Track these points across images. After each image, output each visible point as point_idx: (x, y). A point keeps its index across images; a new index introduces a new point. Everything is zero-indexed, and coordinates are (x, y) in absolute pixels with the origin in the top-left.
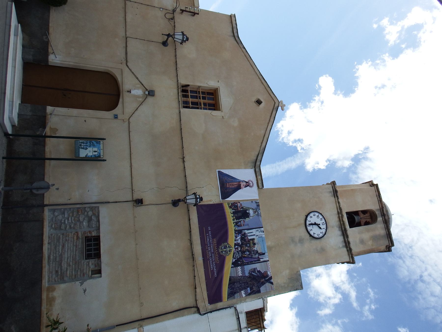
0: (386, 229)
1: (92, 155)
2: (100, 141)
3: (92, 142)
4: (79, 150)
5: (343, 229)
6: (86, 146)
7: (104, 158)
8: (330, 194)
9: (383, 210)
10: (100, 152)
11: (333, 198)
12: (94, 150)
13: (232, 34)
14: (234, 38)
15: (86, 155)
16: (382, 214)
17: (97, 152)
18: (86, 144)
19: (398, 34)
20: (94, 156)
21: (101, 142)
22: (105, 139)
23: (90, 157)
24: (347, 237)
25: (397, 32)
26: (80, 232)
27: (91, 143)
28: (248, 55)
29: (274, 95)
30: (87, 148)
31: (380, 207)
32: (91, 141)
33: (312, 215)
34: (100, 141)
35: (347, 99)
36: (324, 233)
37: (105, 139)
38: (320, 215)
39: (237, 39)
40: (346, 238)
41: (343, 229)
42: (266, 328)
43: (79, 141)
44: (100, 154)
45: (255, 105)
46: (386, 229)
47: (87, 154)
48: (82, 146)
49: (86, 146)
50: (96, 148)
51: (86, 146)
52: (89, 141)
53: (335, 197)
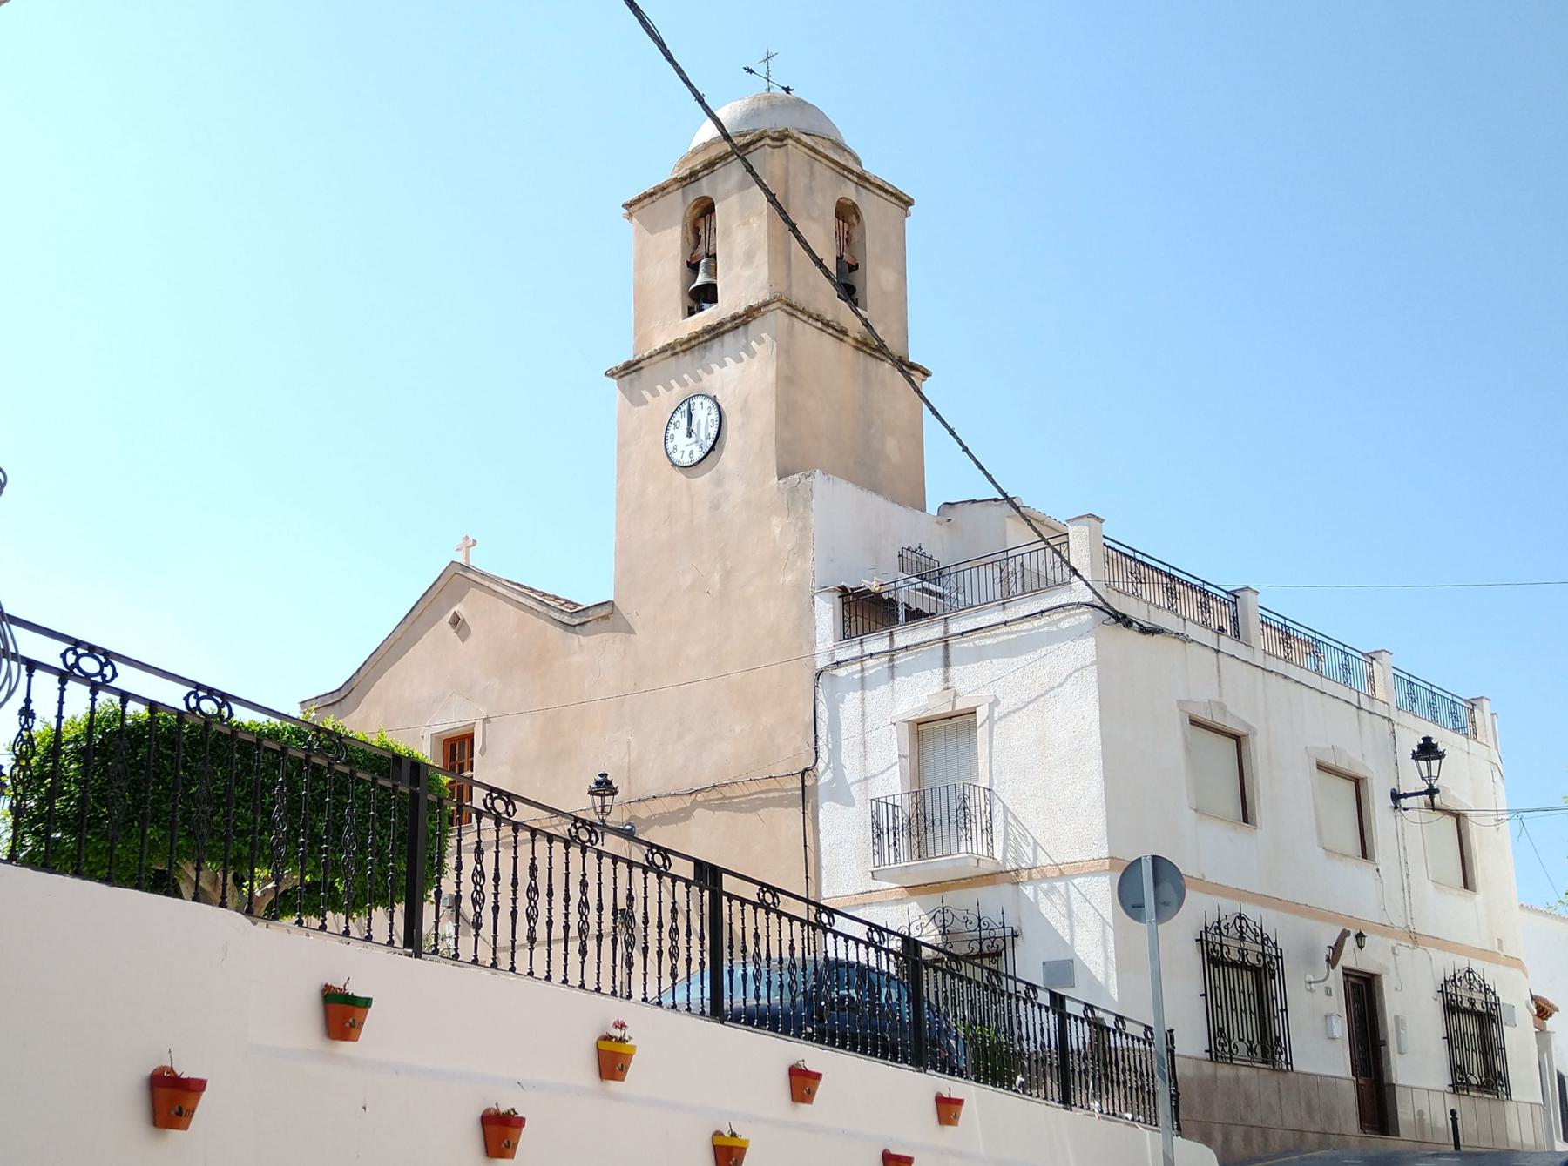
0: (728, 161)
5: (707, 337)
8: (636, 383)
9: (684, 179)
11: (643, 371)
13: (338, 705)
14: (343, 701)
16: (693, 179)
26: (1217, 1126)
28: (438, 584)
29: (439, 578)
31: (678, 189)
33: (686, 461)
35: (59, 655)
36: (694, 458)
38: (670, 449)
39: (343, 694)
40: (726, 327)
41: (707, 337)
45: (132, 1103)
46: (728, 161)
53: (641, 368)
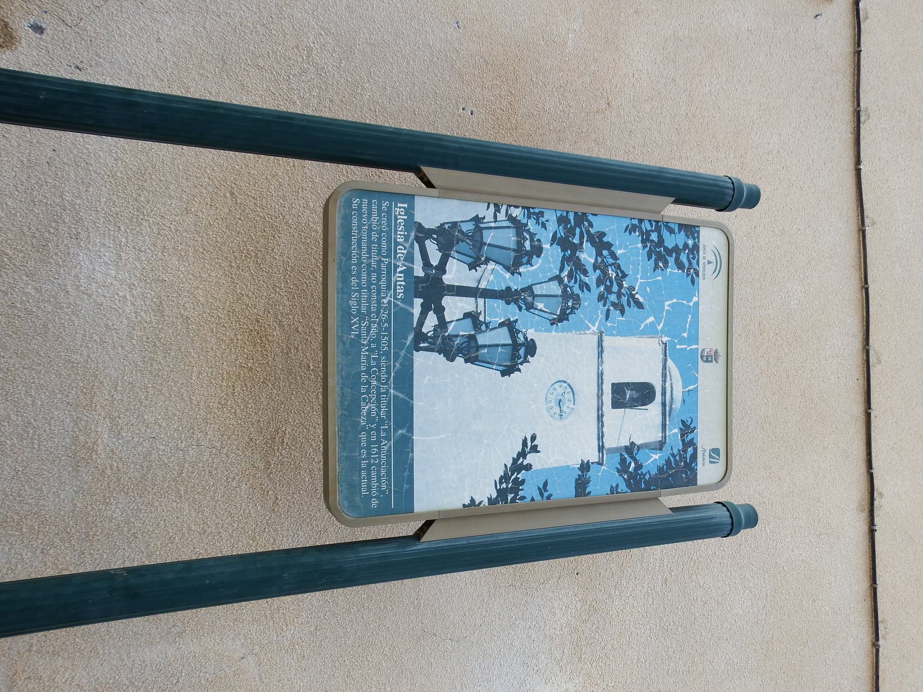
1: (594, 457)
2: (690, 229)
3: (600, 243)
4: (405, 381)
6: (508, 296)
7: (734, 494)
10: (691, 397)
12: (616, 373)
15: (518, 466)
17: (654, 409)
18: (513, 268)
19: (481, 266)
20: (623, 467)
21: (710, 240)
22: (752, 199)
23: (563, 491)
24: (603, 426)
25: (480, 267)
27: (587, 256)
30: (531, 334)
32: (581, 218)
34: (690, 229)
37: (752, 199)
42: (487, 498)
43: (400, 209)
44: (687, 429)
47: (530, 446)
48: (455, 307)
49: (508, 296)
50: (651, 331)
51: (512, 312)
52: (551, 217)
